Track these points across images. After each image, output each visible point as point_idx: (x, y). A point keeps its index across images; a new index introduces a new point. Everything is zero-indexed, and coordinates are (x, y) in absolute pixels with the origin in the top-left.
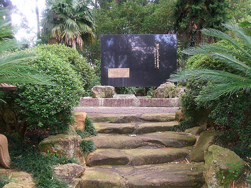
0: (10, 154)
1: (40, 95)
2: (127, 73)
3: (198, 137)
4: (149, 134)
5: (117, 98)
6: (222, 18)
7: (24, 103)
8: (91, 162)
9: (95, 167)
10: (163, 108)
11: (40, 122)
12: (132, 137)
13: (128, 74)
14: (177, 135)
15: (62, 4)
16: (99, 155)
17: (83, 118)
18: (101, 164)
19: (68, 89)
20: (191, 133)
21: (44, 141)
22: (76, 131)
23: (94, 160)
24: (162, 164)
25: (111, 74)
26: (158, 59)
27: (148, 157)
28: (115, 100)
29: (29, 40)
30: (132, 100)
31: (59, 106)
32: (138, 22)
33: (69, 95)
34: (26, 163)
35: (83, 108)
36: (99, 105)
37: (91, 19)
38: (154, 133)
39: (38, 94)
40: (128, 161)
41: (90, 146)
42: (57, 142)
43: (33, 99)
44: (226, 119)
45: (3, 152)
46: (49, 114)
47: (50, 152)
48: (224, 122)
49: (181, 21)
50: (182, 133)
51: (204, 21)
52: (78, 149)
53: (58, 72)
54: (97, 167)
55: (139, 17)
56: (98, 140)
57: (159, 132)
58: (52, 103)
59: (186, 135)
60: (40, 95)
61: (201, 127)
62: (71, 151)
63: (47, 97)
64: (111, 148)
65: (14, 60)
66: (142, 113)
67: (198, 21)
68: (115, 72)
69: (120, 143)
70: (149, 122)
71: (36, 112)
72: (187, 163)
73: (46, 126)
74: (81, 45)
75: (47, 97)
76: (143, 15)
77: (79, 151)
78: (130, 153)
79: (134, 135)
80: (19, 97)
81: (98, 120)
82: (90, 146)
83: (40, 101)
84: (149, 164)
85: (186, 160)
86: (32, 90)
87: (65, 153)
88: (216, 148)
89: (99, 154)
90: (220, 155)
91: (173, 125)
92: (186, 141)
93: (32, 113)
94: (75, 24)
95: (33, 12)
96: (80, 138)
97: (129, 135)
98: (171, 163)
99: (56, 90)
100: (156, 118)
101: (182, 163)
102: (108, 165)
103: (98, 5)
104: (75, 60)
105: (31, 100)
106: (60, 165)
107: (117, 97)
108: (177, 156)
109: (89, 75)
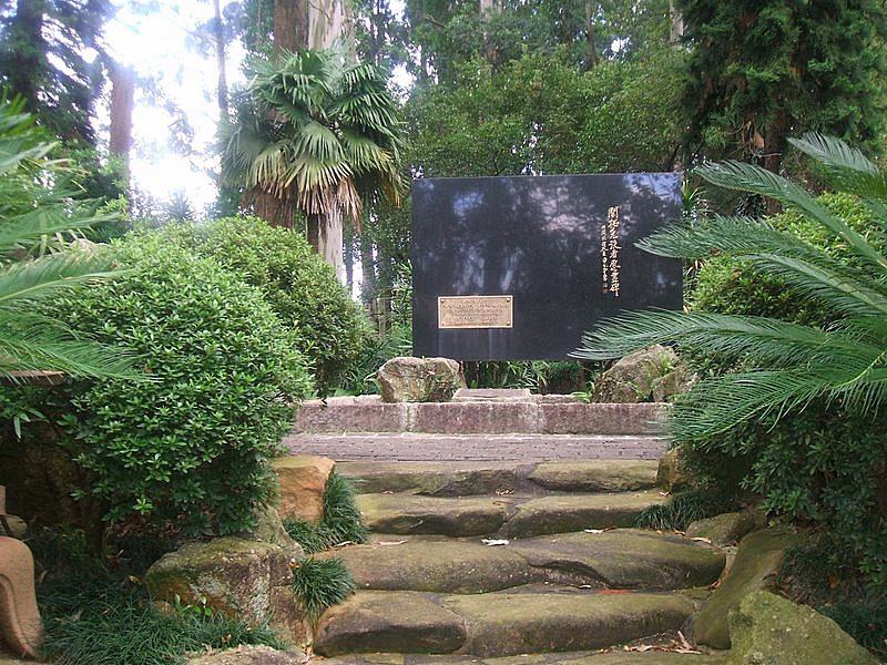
0: (40, 609)
1: (144, 402)
2: (505, 311)
3: (731, 553)
4: (556, 539)
5: (464, 404)
6: (856, 107)
7: (91, 429)
8: (329, 641)
9: (345, 658)
10: (627, 437)
11: (143, 496)
12: (496, 550)
14: (655, 544)
15: (287, 78)
16: (360, 615)
17: (317, 478)
18: (367, 648)
19: (244, 384)
20: (707, 538)
21: (162, 565)
22: (288, 526)
23: (342, 632)
24: (589, 653)
25: (448, 315)
26: (614, 262)
27: (538, 624)
28: (456, 410)
29: (785, 59)
30: (517, 410)
31: (210, 440)
32: (561, 128)
33: (246, 402)
34: (91, 640)
35: (344, 435)
36: (398, 427)
37: (388, 122)
38: (576, 534)
39: (136, 401)
40: (464, 639)
41: (329, 582)
42: (208, 568)
43: (117, 418)
44: (805, 497)
45: (15, 601)
46: (170, 469)
47: (183, 603)
48: (797, 505)
49: (708, 124)
50: (678, 534)
51: (793, 121)
52: (288, 592)
53: (211, 322)
54: (352, 657)
55: (567, 111)
56: (365, 558)
57: (595, 531)
58: (181, 432)
59: (688, 542)
60: (143, 403)
61: (747, 514)
62: (260, 600)
63: (164, 411)
64: (399, 589)
65: (34, 285)
66: (539, 460)
67: (769, 121)
68: (462, 309)
69: (443, 570)
70: (561, 495)
71: (126, 463)
72: (681, 652)
73: (165, 508)
74: (354, 212)
75: (164, 411)
76: (579, 105)
77: (290, 600)
78: (475, 611)
79: (500, 542)
80: (72, 409)
81: (374, 485)
82: (329, 582)
83: (142, 425)
84: (539, 651)
85: (679, 640)
86: (117, 387)
87: (234, 607)
88: (767, 602)
89: (361, 610)
90: (779, 633)
91: (647, 504)
92: (685, 566)
93: (116, 463)
94: (331, 140)
95: (209, 100)
96: (297, 553)
97: (484, 541)
98: (623, 647)
99: (198, 387)
100: (586, 477)
101: (665, 647)
102: (392, 652)
103: (430, 70)
104: (294, 273)
105: (113, 420)
106: (211, 651)
107: (465, 397)
108: (647, 623)
109: (342, 327)
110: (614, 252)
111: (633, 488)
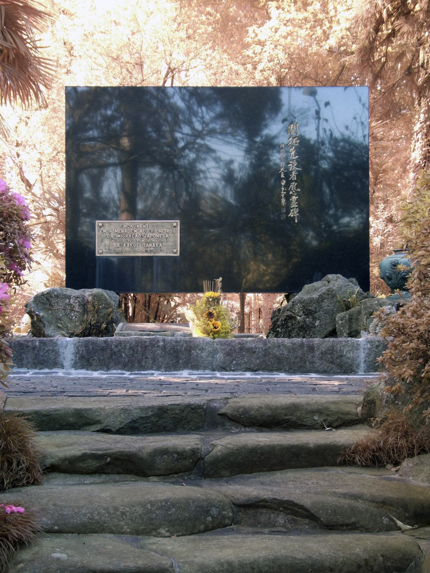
13: (175, 242)
25: (107, 242)
26: (293, 185)
66: (228, 395)
110: (294, 173)
111: (335, 425)
